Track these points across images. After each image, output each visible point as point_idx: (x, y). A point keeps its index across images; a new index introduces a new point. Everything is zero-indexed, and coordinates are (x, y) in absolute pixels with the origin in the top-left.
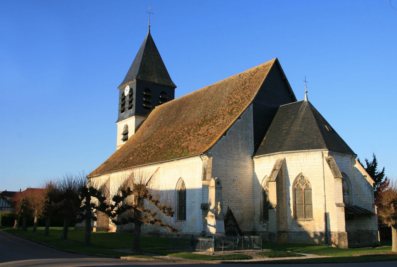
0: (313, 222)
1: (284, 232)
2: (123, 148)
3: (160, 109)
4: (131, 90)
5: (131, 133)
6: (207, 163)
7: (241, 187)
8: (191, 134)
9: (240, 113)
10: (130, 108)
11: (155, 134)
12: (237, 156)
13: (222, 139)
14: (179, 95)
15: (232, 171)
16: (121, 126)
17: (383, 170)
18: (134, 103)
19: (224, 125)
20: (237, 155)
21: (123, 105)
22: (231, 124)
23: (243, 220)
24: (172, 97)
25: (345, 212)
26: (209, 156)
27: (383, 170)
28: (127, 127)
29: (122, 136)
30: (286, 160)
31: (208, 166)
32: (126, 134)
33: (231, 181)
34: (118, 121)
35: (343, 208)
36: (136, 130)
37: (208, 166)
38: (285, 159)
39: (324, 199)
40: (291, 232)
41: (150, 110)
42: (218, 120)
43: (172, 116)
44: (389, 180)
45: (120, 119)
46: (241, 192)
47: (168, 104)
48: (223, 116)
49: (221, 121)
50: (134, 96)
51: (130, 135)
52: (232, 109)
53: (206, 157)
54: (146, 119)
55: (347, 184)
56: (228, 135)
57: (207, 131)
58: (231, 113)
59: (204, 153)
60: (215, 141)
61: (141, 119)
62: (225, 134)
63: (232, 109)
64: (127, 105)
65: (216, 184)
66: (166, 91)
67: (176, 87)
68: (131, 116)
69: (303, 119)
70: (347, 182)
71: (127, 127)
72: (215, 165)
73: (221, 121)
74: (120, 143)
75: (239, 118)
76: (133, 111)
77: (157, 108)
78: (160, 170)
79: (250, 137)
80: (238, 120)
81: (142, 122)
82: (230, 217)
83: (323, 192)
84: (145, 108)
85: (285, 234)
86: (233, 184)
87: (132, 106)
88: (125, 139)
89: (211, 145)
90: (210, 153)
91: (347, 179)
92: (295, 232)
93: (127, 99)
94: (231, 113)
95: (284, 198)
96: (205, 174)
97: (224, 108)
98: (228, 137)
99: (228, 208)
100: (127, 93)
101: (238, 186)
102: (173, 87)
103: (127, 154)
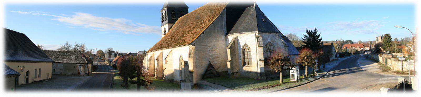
0: (251, 67)
1: (237, 72)
2: (164, 38)
4: (165, 12)
5: (167, 32)
7: (218, 51)
8: (189, 33)
9: (213, 21)
10: (166, 20)
12: (214, 36)
13: (201, 36)
15: (211, 44)
16: (163, 28)
17: (320, 34)
18: (167, 18)
19: (204, 27)
20: (215, 35)
21: (163, 19)
23: (220, 66)
25: (264, 63)
26: (193, 45)
27: (320, 34)
28: (165, 29)
29: (164, 33)
30: (238, 37)
31: (192, 51)
32: (165, 32)
33: (211, 49)
34: (161, 26)
35: (263, 61)
36: (169, 30)
37: (192, 51)
38: (237, 37)
39: (256, 56)
40: (241, 72)
42: (202, 25)
43: (184, 22)
44: (301, 45)
45: (162, 25)
46: (218, 53)
48: (205, 23)
49: (203, 25)
50: (167, 15)
51: (166, 32)
52: (210, 19)
53: (191, 46)
54: (174, 25)
56: (205, 33)
57: (196, 31)
58: (209, 21)
60: (197, 37)
61: (171, 25)
62: (203, 33)
64: (164, 19)
68: (166, 24)
69: (251, 15)
71: (165, 29)
75: (212, 24)
76: (167, 21)
79: (224, 25)
80: (211, 25)
82: (210, 66)
83: (256, 53)
85: (237, 73)
86: (213, 50)
87: (166, 19)
88: (165, 34)
89: (194, 39)
90: (193, 43)
91: (273, 45)
92: (243, 72)
93: (164, 16)
94: (209, 21)
95: (236, 56)
97: (207, 18)
98: (205, 34)
99: (210, 61)
100: (164, 14)
101: (216, 51)
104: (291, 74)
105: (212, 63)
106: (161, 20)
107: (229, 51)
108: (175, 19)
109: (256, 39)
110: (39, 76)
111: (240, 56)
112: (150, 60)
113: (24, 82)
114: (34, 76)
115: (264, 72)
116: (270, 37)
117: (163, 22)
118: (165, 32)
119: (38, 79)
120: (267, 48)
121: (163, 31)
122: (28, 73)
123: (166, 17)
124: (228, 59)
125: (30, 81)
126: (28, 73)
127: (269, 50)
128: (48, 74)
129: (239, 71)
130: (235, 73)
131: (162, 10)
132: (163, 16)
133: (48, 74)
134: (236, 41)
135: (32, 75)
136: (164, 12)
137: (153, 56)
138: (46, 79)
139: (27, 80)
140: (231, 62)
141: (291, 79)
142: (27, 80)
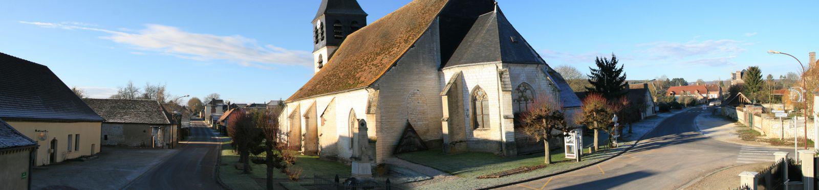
1: (461, 141)
2: (319, 74)
3: (350, 38)
4: (322, 24)
5: (325, 62)
6: (373, 96)
8: (368, 64)
9: (414, 41)
10: (322, 40)
11: (343, 62)
13: (391, 70)
14: (370, 21)
16: (316, 55)
18: (325, 35)
19: (396, 54)
21: (317, 37)
22: (403, 53)
24: (365, 25)
25: (514, 123)
26: (376, 89)
28: (321, 56)
29: (318, 64)
32: (321, 62)
34: (314, 52)
36: (329, 59)
39: (498, 110)
41: (342, 39)
42: (394, 49)
43: (358, 44)
45: (315, 50)
47: (357, 33)
49: (396, 49)
50: (324, 29)
51: (324, 63)
52: (409, 36)
53: (373, 90)
55: (532, 92)
57: (381, 60)
58: (406, 41)
59: (369, 86)
60: (382, 73)
61: (333, 48)
62: (395, 64)
63: (409, 36)
64: (320, 37)
65: (360, 126)
66: (360, 19)
67: (367, 15)
68: (323, 47)
70: (530, 90)
71: (321, 56)
72: (382, 97)
73: (396, 49)
74: (317, 70)
75: (413, 46)
76: (324, 42)
77: (349, 37)
78: (336, 100)
80: (411, 49)
81: (336, 50)
82: (409, 129)
83: (498, 104)
84: (336, 38)
87: (323, 37)
88: (320, 67)
89: (378, 77)
90: (376, 85)
93: (320, 31)
95: (460, 110)
96: (369, 107)
97: (402, 35)
98: (399, 67)
99: (408, 120)
100: (319, 27)
101: (419, 99)
102: (364, 16)
103: (316, 83)
104: (566, 144)
105: (412, 124)
106: (314, 39)
107: (445, 100)
108: (341, 38)
109: (498, 77)
110: (76, 150)
111: (468, 110)
112: (291, 117)
113: (47, 161)
114: (66, 150)
115: (514, 140)
116: (525, 72)
117: (317, 42)
118: (321, 62)
119: (74, 155)
120: (520, 94)
121: (317, 60)
122: (54, 142)
123: (322, 34)
124: (443, 117)
125: (59, 159)
126: (54, 142)
127: (523, 99)
128: (93, 145)
129: (464, 139)
130: (456, 142)
131: (315, 20)
132: (317, 32)
133: (93, 145)
134: (459, 81)
135: (61, 148)
136: (319, 23)
137: (298, 110)
138: (89, 154)
139: (53, 157)
140: (450, 121)
141: (566, 154)
142: (53, 157)
